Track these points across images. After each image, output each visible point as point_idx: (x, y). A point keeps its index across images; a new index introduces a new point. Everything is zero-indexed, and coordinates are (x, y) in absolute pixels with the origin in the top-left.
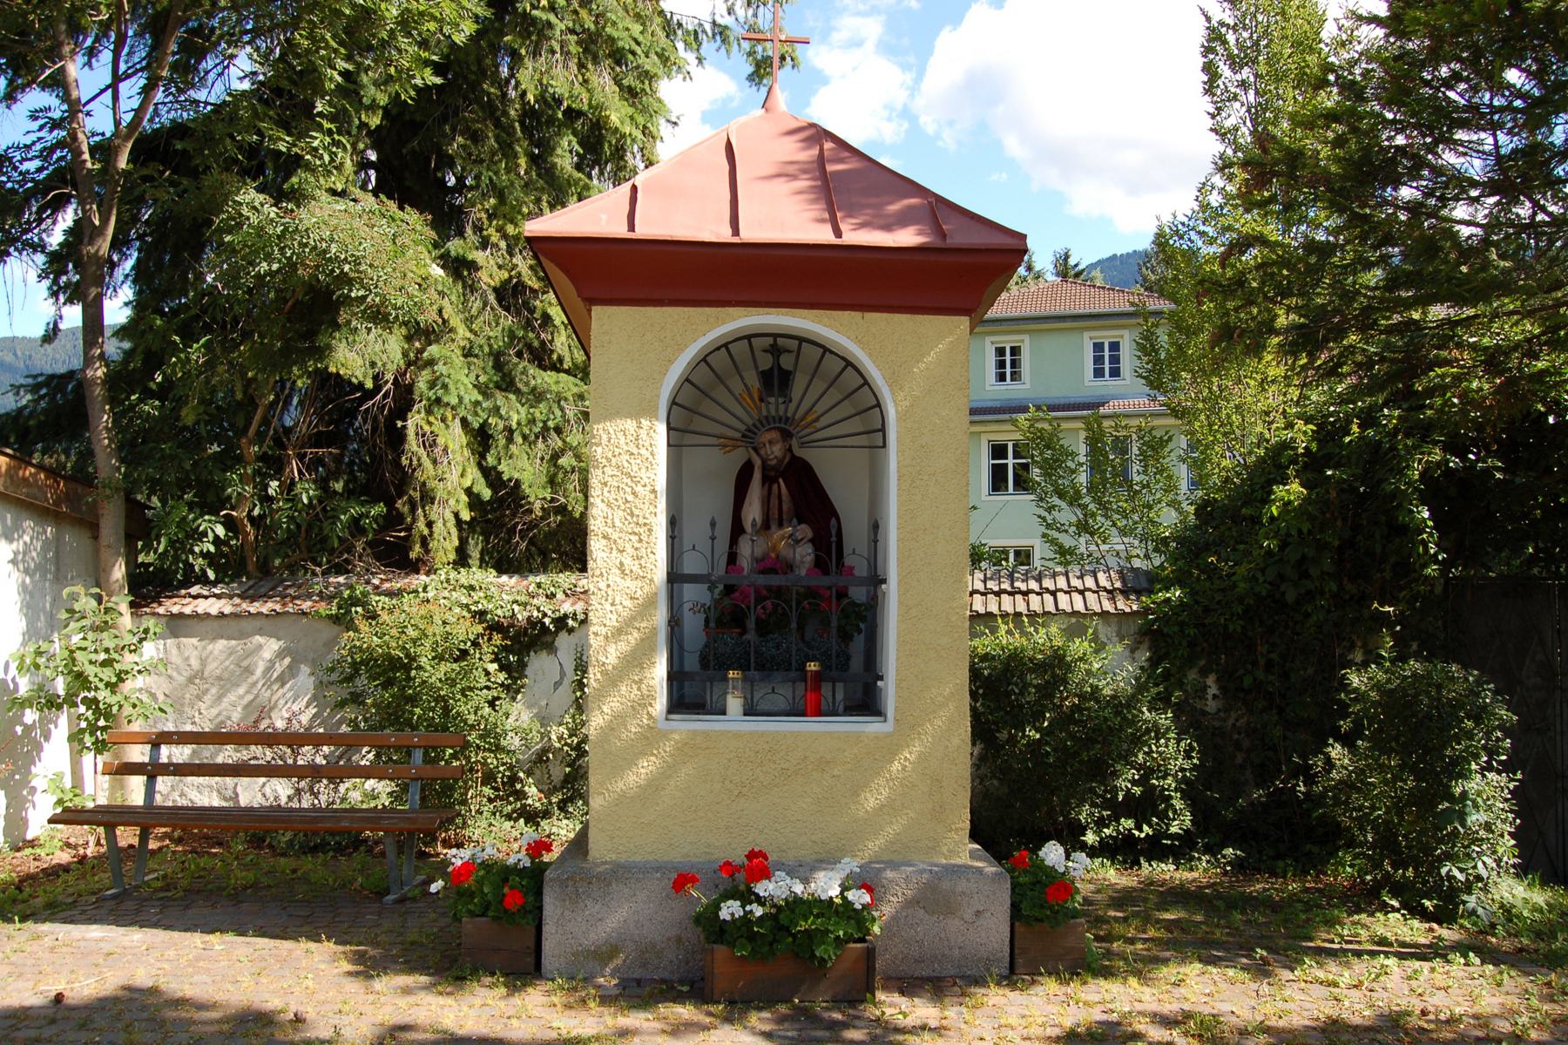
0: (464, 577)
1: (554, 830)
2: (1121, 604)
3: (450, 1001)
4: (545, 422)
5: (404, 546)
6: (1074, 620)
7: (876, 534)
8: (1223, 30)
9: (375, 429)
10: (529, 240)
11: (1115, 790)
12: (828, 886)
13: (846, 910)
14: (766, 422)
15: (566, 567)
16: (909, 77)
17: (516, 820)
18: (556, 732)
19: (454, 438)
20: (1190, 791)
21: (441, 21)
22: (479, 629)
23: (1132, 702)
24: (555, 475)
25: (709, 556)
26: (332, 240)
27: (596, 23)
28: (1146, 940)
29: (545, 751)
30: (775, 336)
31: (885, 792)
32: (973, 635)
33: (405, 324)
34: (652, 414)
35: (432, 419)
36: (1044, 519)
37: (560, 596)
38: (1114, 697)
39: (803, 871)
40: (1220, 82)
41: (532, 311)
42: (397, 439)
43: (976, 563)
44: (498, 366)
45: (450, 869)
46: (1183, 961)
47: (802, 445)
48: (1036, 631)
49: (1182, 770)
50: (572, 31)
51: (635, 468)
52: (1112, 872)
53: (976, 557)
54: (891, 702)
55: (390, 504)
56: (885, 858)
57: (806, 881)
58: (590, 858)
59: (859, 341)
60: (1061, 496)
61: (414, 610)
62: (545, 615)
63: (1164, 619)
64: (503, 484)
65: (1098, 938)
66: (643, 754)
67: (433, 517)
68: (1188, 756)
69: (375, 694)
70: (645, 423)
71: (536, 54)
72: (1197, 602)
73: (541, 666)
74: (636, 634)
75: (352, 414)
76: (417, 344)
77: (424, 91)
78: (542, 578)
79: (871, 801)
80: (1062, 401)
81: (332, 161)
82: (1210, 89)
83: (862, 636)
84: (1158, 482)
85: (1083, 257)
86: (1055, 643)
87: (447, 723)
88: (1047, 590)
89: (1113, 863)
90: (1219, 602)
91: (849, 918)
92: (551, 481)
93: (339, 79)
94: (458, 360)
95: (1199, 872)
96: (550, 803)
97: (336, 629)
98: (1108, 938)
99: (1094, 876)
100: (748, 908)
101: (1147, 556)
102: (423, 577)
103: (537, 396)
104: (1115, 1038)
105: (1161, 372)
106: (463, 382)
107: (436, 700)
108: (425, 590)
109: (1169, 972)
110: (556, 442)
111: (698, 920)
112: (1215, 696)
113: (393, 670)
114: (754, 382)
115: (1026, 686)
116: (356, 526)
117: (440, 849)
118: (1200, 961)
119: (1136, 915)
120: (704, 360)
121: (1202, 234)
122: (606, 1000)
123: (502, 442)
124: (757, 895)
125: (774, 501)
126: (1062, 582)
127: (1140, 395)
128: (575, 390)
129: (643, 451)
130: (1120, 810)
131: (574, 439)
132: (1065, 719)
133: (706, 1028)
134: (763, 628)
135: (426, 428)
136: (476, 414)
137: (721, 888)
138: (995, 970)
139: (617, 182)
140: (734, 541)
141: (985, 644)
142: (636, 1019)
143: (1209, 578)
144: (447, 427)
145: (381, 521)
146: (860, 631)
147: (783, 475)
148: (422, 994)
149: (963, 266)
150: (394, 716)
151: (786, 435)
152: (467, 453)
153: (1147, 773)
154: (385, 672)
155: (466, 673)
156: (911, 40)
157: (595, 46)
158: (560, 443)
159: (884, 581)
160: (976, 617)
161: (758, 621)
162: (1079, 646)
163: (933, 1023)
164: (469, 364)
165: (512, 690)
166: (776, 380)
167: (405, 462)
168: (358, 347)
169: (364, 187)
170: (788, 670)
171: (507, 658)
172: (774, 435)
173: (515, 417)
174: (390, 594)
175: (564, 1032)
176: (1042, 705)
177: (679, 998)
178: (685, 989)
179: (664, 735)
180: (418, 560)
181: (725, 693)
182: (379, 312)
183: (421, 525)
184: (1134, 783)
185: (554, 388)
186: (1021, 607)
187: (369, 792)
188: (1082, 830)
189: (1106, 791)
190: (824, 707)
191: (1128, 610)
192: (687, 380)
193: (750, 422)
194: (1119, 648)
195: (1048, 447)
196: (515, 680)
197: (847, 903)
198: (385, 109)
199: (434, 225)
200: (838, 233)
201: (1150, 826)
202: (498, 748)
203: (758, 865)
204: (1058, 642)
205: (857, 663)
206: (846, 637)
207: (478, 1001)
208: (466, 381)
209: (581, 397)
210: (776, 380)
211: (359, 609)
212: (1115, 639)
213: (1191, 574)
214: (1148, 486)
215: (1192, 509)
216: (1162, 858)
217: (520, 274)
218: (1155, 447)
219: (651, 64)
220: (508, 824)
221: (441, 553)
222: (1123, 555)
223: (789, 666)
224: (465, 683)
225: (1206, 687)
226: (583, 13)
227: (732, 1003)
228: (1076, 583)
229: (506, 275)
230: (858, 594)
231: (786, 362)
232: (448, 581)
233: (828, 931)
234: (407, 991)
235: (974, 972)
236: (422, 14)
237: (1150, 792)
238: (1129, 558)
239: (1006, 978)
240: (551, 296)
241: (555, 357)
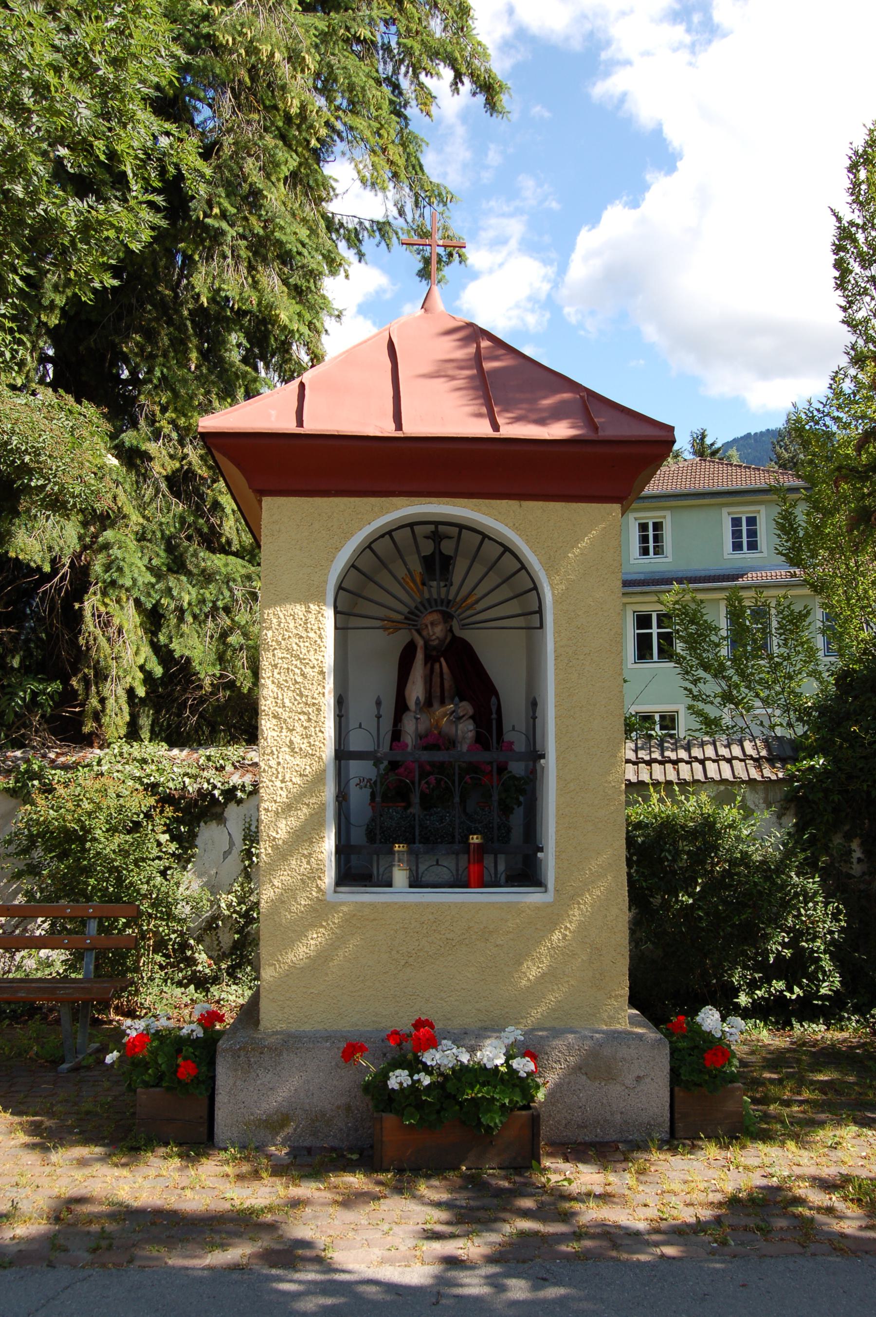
0: (136, 750)
1: (224, 995)
2: (767, 772)
3: (125, 1172)
4: (214, 603)
5: (77, 721)
6: (722, 788)
7: (534, 711)
8: (853, 230)
9: (52, 609)
10: (201, 434)
11: (766, 953)
12: (492, 1055)
13: (510, 1079)
14: (428, 604)
15: (233, 740)
16: (551, 271)
17: (186, 986)
18: (226, 900)
19: (128, 618)
20: (837, 951)
21: (119, 230)
22: (152, 801)
23: (781, 867)
24: (225, 652)
25: (375, 734)
26: (13, 432)
27: (265, 228)
28: (801, 1103)
29: (214, 918)
30: (437, 524)
31: (546, 961)
32: (628, 804)
33: (82, 511)
34: (319, 598)
35: (107, 600)
36: (690, 691)
37: (229, 768)
38: (763, 862)
39: (470, 1037)
40: (851, 278)
41: (201, 496)
42: (75, 619)
43: (632, 740)
44: (170, 549)
45: (125, 1040)
46: (840, 1123)
47: (464, 626)
48: (687, 799)
49: (831, 932)
50: (243, 237)
51: (304, 651)
52: (765, 1032)
53: (629, 728)
54: (551, 874)
55: (66, 682)
56: (548, 1025)
57: (472, 1050)
58: (261, 1027)
59: (516, 528)
60: (706, 667)
61: (89, 783)
62: (215, 787)
63: (808, 786)
64: (177, 662)
65: (755, 1101)
66: (312, 926)
67: (106, 693)
68: (835, 918)
69: (52, 866)
71: (209, 258)
72: (840, 769)
73: (210, 835)
74: (305, 810)
75: (30, 592)
76: (92, 529)
77: (100, 294)
78: (212, 751)
79: (532, 971)
80: (703, 574)
81: (13, 357)
82: (841, 284)
83: (522, 808)
84: (798, 653)
85: (718, 437)
86: (705, 811)
87: (121, 896)
88: (696, 759)
89: (766, 1024)
90: (861, 770)
91: (514, 1085)
92: (221, 658)
93: (20, 283)
94: (132, 545)
95: (848, 1033)
96: (220, 969)
97: (13, 802)
98: (765, 1101)
99: (746, 1036)
100: (416, 1077)
101: (790, 725)
102: (98, 751)
103: (207, 577)
104: (776, 1203)
105: (800, 550)
106: (136, 565)
107: (110, 872)
108: (99, 763)
109: (825, 1135)
110: (225, 621)
111: (367, 1088)
112: (859, 860)
113: (69, 841)
114: (417, 567)
115: (677, 854)
116: (33, 703)
117: (112, 1016)
118: (856, 1122)
119: (789, 1076)
120: (369, 546)
121: (836, 419)
122: (279, 1170)
123: (174, 621)
124: (425, 1064)
125: (436, 680)
126: (710, 751)
127: (778, 567)
128: (243, 571)
129: (312, 635)
130: (770, 973)
131: (242, 618)
132: (716, 885)
133: (376, 1198)
134: (427, 802)
135: (102, 609)
136: (149, 595)
137: (389, 1056)
138: (657, 1136)
139: (286, 380)
140: (398, 719)
141: (638, 812)
142: (307, 1189)
143: (851, 746)
144: (122, 608)
145: (56, 697)
146: (519, 804)
148: (98, 1165)
149: (614, 456)
150: (70, 887)
151: (447, 617)
152: (140, 632)
153: (797, 935)
154: (60, 844)
155: (139, 845)
156: (552, 240)
157: (265, 249)
158: (229, 622)
159: (543, 756)
160: (630, 785)
161: (424, 797)
162: (729, 813)
163: (598, 1190)
164: (142, 548)
165: (182, 860)
166: (438, 565)
167: (82, 641)
168: (36, 532)
169: (42, 381)
171: (178, 828)
172: (436, 617)
173: (187, 598)
174: (65, 767)
175: (237, 1202)
176: (694, 871)
177: (349, 1167)
178: (355, 1157)
179: (333, 907)
180: (91, 734)
181: (392, 866)
182: (57, 500)
183: (94, 702)
184: (784, 945)
185: (223, 570)
186: (672, 776)
187: (46, 962)
188: (735, 992)
189: (757, 954)
190: (486, 878)
191: (774, 778)
192: (353, 566)
193: (413, 605)
194: (767, 815)
195: (692, 622)
196: (185, 849)
197: (512, 1072)
198: (62, 309)
199: (108, 417)
200: (496, 427)
201: (801, 987)
202: (169, 916)
203: (425, 1034)
204: (708, 809)
205: (517, 834)
206: (506, 809)
207: (152, 1172)
208: (140, 564)
209: (249, 578)
210: (438, 565)
211: (36, 783)
212: (763, 806)
213: (834, 742)
214: (788, 658)
215: (832, 680)
216: (813, 1020)
217: (190, 463)
218: (794, 622)
219: (315, 261)
220: (179, 991)
221: (113, 728)
222: (766, 723)
223: (452, 839)
224: (137, 855)
225: (850, 852)
226: (253, 220)
227: (400, 1171)
228: (723, 751)
229: (178, 465)
230: (517, 768)
231: (447, 547)
232: (121, 754)
233: (493, 1098)
234: (83, 1163)
235: (636, 1136)
236: (101, 223)
237: (799, 953)
238: (772, 727)
239: (667, 1142)
240: (221, 485)
241: (223, 540)
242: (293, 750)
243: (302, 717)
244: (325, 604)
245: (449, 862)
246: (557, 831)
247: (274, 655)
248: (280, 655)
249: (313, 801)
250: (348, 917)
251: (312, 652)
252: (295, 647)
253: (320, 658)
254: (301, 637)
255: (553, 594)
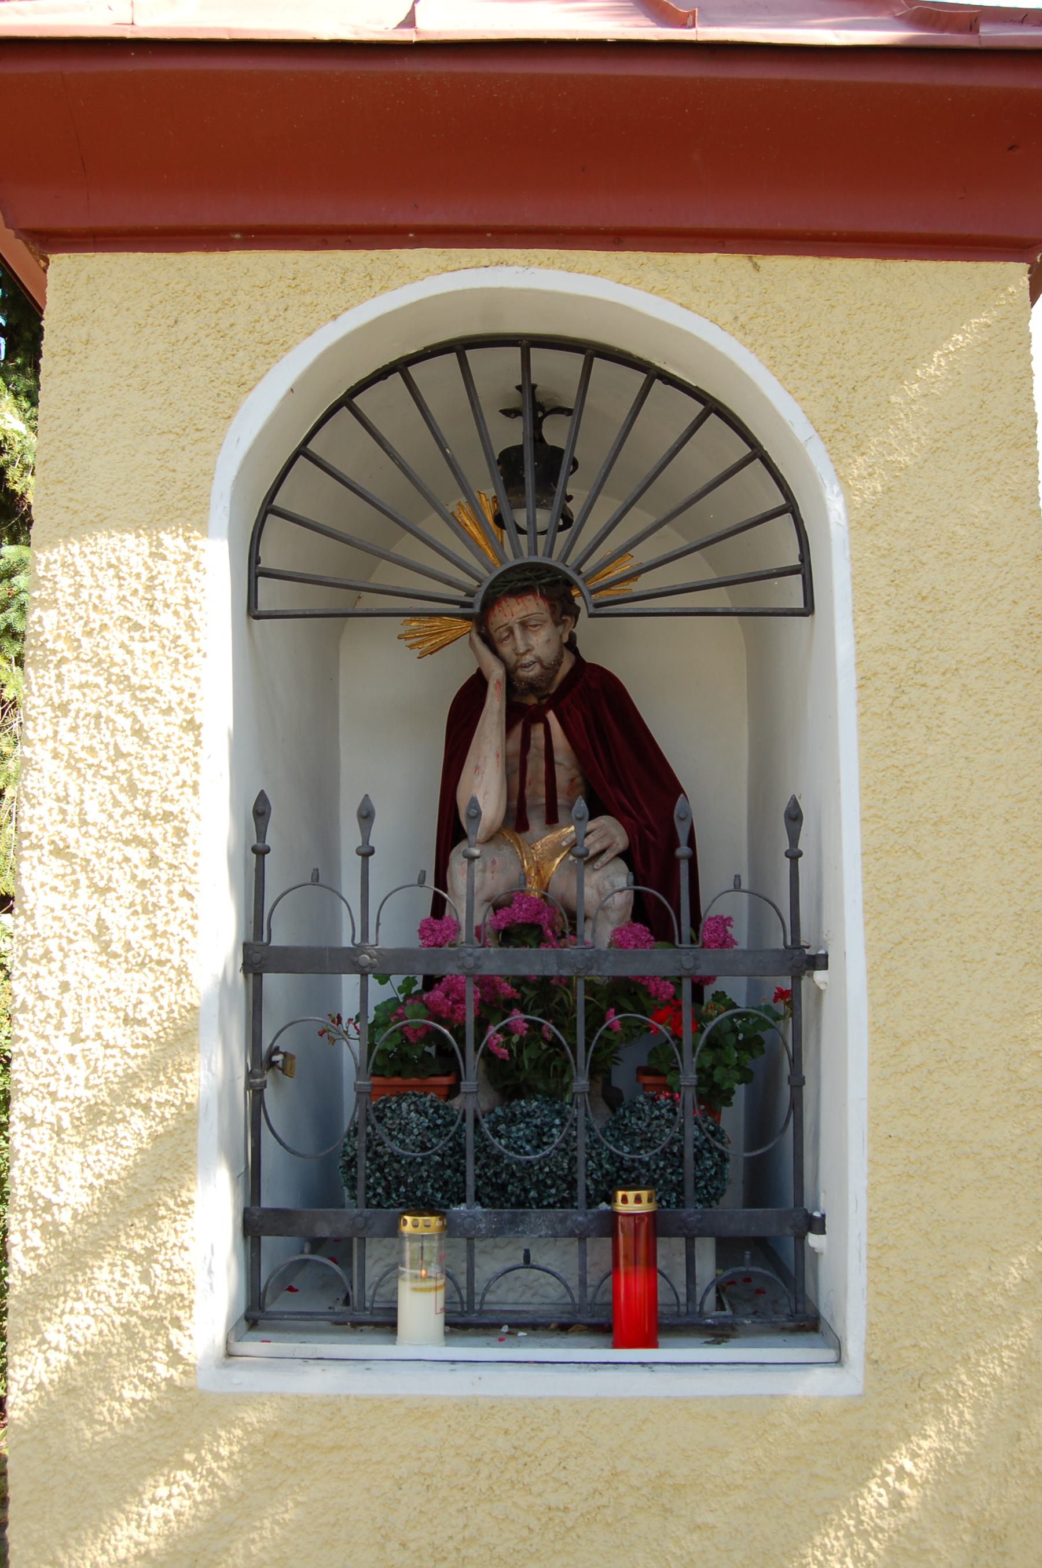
30: (527, 343)
51: (144, 665)
59: (740, 328)
70: (172, 542)
74: (139, 1122)
125: (536, 765)
129: (166, 619)
134: (507, 1080)
147: (555, 702)
170: (566, 1202)
206: (713, 1097)
231: (555, 433)
242: (105, 947)
243: (132, 852)
244: (205, 533)
245: (558, 1257)
246: (873, 1187)
247: (59, 678)
248: (78, 678)
249: (160, 1094)
250: (258, 1438)
251: (166, 669)
252: (120, 655)
253: (189, 686)
254: (137, 627)
255: (849, 506)
